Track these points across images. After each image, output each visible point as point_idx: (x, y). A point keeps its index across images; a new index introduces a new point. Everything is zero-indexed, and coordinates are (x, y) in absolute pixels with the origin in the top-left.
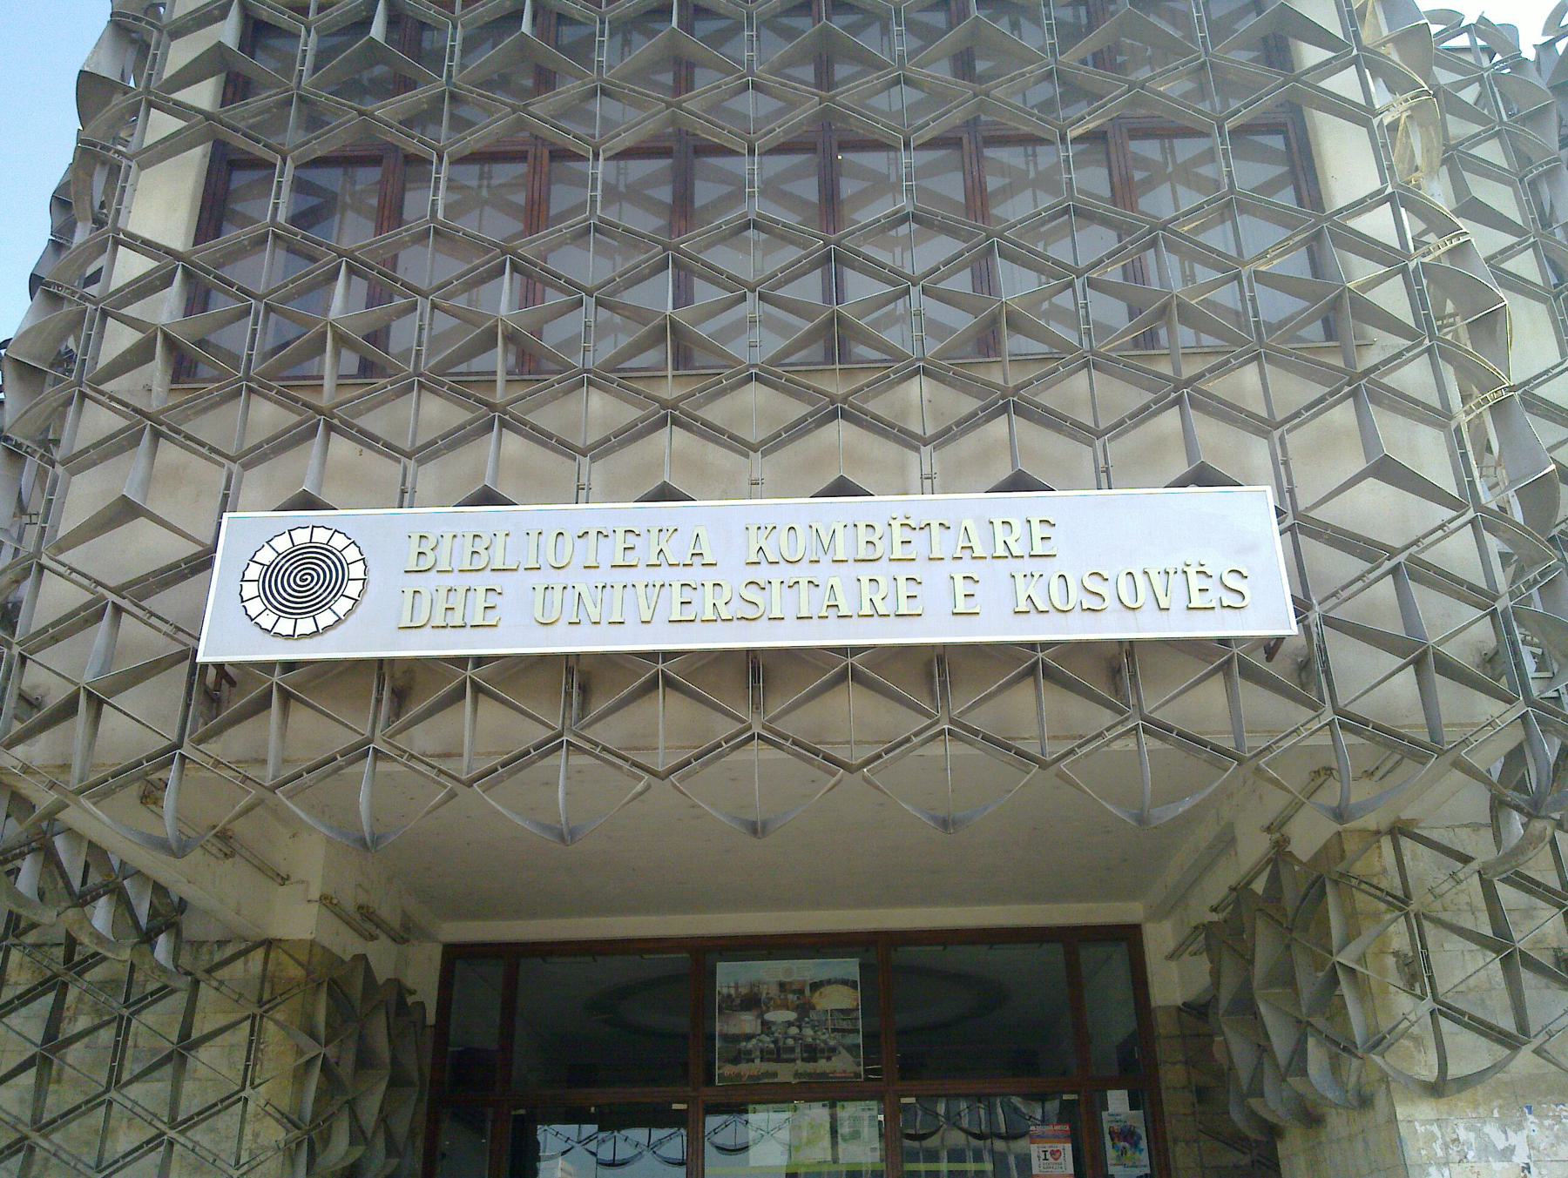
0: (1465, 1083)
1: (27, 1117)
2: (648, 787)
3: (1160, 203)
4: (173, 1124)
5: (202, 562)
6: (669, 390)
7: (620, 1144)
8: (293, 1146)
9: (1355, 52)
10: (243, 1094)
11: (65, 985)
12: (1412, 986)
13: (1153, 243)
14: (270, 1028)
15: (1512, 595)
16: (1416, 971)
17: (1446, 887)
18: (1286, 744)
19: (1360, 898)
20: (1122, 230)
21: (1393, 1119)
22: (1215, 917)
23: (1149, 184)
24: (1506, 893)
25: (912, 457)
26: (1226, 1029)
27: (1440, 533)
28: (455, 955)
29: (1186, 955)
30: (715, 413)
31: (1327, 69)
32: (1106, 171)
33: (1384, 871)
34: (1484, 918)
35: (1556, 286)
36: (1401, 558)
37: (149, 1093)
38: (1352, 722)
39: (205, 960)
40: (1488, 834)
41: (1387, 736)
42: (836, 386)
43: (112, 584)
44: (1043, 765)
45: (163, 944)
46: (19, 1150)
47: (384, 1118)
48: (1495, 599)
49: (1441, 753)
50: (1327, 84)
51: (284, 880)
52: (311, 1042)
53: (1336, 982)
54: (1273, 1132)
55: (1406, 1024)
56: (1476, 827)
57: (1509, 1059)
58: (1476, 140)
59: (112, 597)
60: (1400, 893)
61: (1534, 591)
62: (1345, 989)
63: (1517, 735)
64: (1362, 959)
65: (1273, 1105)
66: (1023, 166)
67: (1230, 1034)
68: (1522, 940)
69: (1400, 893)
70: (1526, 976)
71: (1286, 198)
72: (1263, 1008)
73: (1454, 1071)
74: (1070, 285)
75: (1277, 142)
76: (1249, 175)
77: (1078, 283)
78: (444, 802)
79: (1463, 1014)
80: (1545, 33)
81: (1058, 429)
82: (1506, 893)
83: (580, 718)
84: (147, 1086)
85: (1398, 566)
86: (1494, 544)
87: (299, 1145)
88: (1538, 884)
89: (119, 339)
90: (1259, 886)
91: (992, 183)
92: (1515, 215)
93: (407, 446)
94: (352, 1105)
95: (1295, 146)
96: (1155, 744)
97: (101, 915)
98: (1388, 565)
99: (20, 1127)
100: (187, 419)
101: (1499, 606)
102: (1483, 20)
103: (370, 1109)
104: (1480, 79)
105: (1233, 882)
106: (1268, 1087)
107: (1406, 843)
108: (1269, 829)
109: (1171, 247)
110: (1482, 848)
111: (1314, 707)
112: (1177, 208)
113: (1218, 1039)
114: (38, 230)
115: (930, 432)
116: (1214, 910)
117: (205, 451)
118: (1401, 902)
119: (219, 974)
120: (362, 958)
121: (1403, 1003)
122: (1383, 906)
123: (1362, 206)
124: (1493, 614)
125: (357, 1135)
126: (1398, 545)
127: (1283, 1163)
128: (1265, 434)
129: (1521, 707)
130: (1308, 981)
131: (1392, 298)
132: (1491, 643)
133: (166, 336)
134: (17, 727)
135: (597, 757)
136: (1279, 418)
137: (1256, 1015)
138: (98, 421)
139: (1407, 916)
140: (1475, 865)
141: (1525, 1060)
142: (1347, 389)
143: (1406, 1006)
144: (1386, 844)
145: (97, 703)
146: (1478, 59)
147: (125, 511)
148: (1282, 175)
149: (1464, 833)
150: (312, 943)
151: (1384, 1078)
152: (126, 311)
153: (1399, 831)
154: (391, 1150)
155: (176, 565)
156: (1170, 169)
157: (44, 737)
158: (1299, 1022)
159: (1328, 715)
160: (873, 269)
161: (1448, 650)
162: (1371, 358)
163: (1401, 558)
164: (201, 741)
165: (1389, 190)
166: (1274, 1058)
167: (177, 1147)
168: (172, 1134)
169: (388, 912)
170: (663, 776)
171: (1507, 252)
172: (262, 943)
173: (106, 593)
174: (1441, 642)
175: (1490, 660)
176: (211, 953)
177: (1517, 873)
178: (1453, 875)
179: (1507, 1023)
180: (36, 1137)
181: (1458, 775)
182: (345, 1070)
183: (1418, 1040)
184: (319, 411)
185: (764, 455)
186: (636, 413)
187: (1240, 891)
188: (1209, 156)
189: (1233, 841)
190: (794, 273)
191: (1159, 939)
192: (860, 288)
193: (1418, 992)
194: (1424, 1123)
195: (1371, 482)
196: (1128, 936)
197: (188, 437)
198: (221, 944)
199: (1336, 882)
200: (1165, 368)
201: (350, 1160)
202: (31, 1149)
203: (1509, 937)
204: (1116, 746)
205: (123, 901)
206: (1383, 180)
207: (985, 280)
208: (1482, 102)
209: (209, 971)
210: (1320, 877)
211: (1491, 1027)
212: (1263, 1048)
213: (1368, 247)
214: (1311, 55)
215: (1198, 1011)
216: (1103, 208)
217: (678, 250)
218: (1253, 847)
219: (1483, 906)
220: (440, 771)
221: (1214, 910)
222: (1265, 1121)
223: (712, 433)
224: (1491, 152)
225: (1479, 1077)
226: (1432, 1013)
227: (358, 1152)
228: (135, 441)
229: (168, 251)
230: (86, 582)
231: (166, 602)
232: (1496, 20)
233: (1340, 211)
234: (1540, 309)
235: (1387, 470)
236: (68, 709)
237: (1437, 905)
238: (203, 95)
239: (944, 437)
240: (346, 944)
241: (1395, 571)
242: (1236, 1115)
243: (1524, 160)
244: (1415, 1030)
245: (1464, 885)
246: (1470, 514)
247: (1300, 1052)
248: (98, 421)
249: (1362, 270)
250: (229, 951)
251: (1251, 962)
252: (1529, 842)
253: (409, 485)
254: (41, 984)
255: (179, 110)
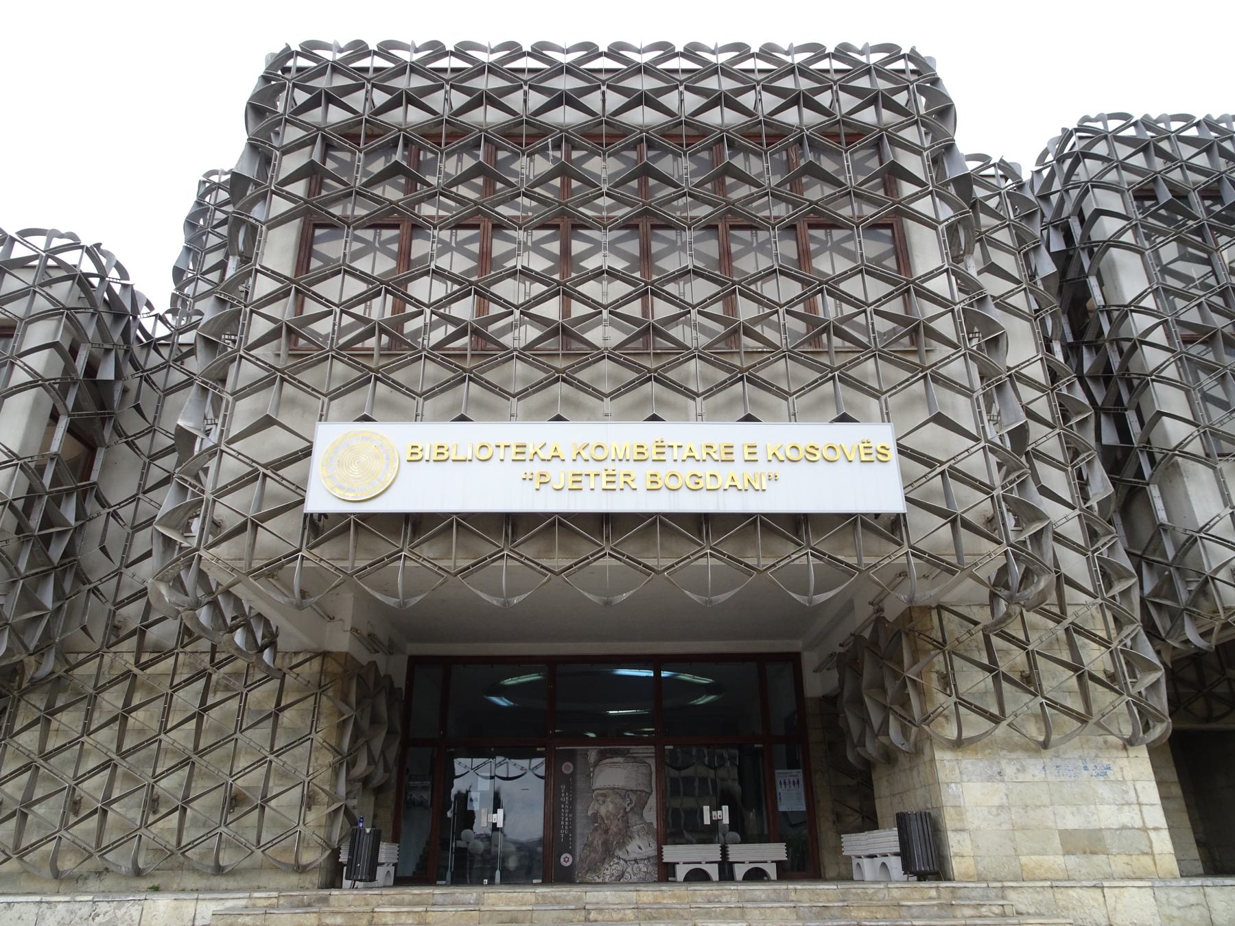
0: (971, 740)
1: (191, 746)
2: (549, 580)
3: (824, 264)
4: (272, 752)
5: (307, 453)
6: (560, 364)
7: (511, 767)
8: (337, 765)
9: (931, 188)
10: (311, 736)
11: (210, 675)
12: (945, 690)
13: (821, 291)
14: (324, 699)
15: (1003, 487)
16: (947, 681)
17: (965, 637)
18: (886, 562)
19: (920, 642)
20: (804, 282)
21: (933, 760)
22: (842, 650)
23: (818, 252)
24: (996, 642)
25: (691, 402)
26: (846, 710)
27: (966, 454)
28: (415, 662)
29: (825, 671)
30: (584, 376)
31: (916, 197)
32: (795, 243)
33: (933, 628)
34: (985, 654)
35: (1036, 311)
36: (945, 467)
37: (259, 736)
38: (918, 553)
39: (287, 664)
40: (988, 610)
41: (934, 561)
42: (650, 363)
43: (262, 463)
44: (759, 572)
45: (267, 655)
46: (188, 764)
47: (383, 752)
48: (993, 489)
49: (963, 570)
50: (914, 206)
51: (332, 619)
52: (347, 708)
53: (906, 687)
54: (869, 765)
55: (941, 709)
56: (982, 605)
57: (994, 729)
58: (996, 229)
59: (262, 470)
60: (941, 640)
61: (1014, 485)
62: (910, 690)
63: (1002, 561)
64: (919, 674)
65: (871, 749)
66: (750, 240)
67: (848, 713)
68: (1003, 666)
69: (941, 640)
70: (1005, 685)
71: (891, 263)
72: (866, 699)
73: (965, 735)
74: (777, 312)
75: (888, 232)
76: (873, 248)
77: (781, 311)
78: (442, 584)
79: (971, 704)
80: (1037, 164)
81: (769, 391)
82: (996, 642)
83: (513, 542)
84: (257, 731)
85: (944, 470)
86: (993, 459)
87: (341, 764)
88: (1014, 637)
89: (260, 327)
90: (867, 634)
91: (735, 248)
92: (1015, 273)
93: (419, 391)
94: (367, 743)
95: (896, 235)
96: (817, 561)
97: (239, 637)
98: (939, 470)
99: (109, 753)
100: (299, 372)
101: (995, 493)
102: (1002, 160)
103: (377, 744)
104: (999, 194)
105: (852, 630)
106: (868, 744)
107: (945, 614)
108: (871, 604)
109: (830, 294)
110: (983, 616)
111: (900, 545)
112: (823, 194)
113: (841, 715)
114: (178, 240)
115: (701, 391)
116: (841, 645)
117: (309, 390)
118: (941, 645)
119: (296, 670)
120: (373, 664)
121: (941, 698)
122: (931, 647)
123: (932, 275)
124: (992, 497)
125: (371, 761)
126: (944, 460)
127: (875, 783)
128: (878, 398)
129: (1005, 548)
130: (891, 687)
131: (945, 326)
132: (990, 513)
133: (287, 326)
134: (211, 539)
135: (522, 563)
136: (884, 390)
137: (862, 703)
138: (249, 372)
139: (944, 652)
140: (980, 626)
141: (1002, 729)
142: (920, 375)
143: (941, 699)
144: (934, 614)
145: (255, 526)
146: (998, 182)
147: (267, 422)
148: (887, 251)
149: (975, 609)
150: (347, 653)
151: (930, 738)
152: (261, 311)
153: (940, 608)
154: (386, 769)
155: (296, 453)
156: (829, 244)
157: (224, 545)
158: (885, 707)
159: (906, 549)
160: (670, 299)
161: (966, 516)
162: (934, 358)
163: (945, 467)
164: (312, 547)
165: (946, 267)
166: (872, 727)
167: (273, 764)
168: (271, 757)
169: (381, 634)
170: (557, 574)
171: (1011, 293)
172: (316, 655)
173: (259, 468)
174: (963, 512)
175: (990, 521)
176: (291, 659)
177: (1002, 631)
178: (969, 632)
179: (995, 710)
180: (195, 758)
181: (970, 582)
182: (365, 723)
183: (946, 717)
184: (371, 370)
185: (611, 399)
186: (543, 375)
187: (857, 637)
188: (849, 238)
189: (852, 608)
190: (627, 300)
191: (810, 660)
192: (663, 309)
193: (948, 692)
194: (949, 761)
195: (931, 424)
196: (793, 659)
197: (300, 382)
198: (296, 653)
199: (907, 634)
200: (825, 360)
201: (368, 773)
202: (116, 766)
203: (996, 663)
204: (797, 562)
205: (250, 632)
206: (943, 261)
207: (731, 308)
208: (1000, 207)
209: (291, 668)
210: (899, 631)
211: (986, 712)
212: (865, 721)
213: (934, 298)
214: (908, 189)
215: (830, 701)
216: (794, 270)
217: (565, 286)
218: (863, 613)
219: (984, 648)
220: (440, 568)
221: (841, 645)
222: (864, 759)
223: (583, 387)
224: (1003, 236)
225: (980, 737)
226: (955, 703)
227: (372, 768)
228: (272, 382)
229: (286, 278)
230: (248, 461)
231: (288, 472)
232: (1008, 161)
233: (920, 278)
234: (1026, 324)
235: (940, 419)
236: (241, 529)
237: (961, 647)
238: (299, 188)
239: (709, 393)
240: (364, 657)
241: (942, 473)
242: (851, 757)
243: (1021, 240)
244: (946, 712)
245: (974, 637)
246: (982, 444)
247: (885, 723)
248: (249, 372)
249: (931, 309)
250: (300, 658)
251: (861, 675)
252: (1008, 615)
253: (420, 412)
254: (197, 674)
255: (289, 197)
